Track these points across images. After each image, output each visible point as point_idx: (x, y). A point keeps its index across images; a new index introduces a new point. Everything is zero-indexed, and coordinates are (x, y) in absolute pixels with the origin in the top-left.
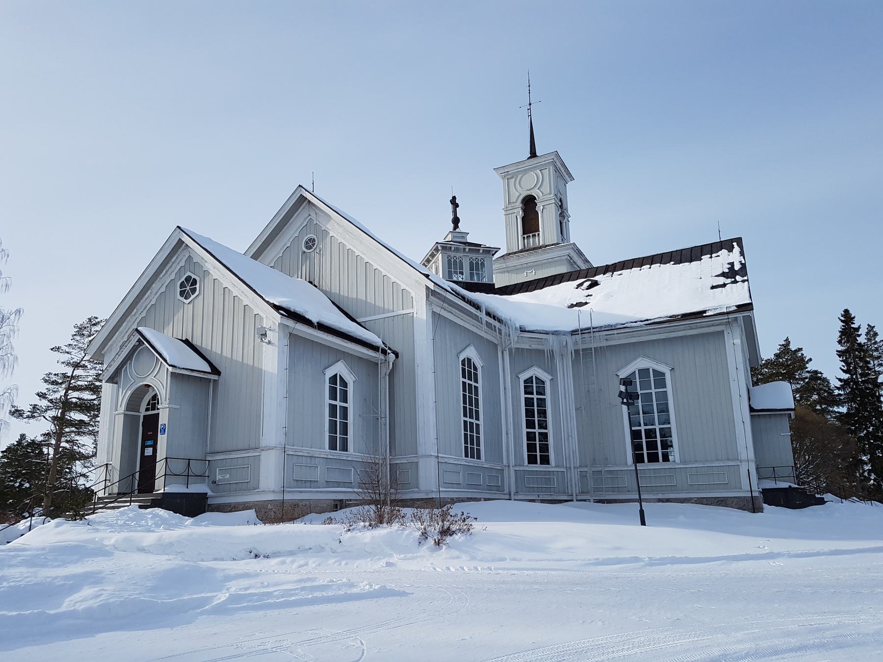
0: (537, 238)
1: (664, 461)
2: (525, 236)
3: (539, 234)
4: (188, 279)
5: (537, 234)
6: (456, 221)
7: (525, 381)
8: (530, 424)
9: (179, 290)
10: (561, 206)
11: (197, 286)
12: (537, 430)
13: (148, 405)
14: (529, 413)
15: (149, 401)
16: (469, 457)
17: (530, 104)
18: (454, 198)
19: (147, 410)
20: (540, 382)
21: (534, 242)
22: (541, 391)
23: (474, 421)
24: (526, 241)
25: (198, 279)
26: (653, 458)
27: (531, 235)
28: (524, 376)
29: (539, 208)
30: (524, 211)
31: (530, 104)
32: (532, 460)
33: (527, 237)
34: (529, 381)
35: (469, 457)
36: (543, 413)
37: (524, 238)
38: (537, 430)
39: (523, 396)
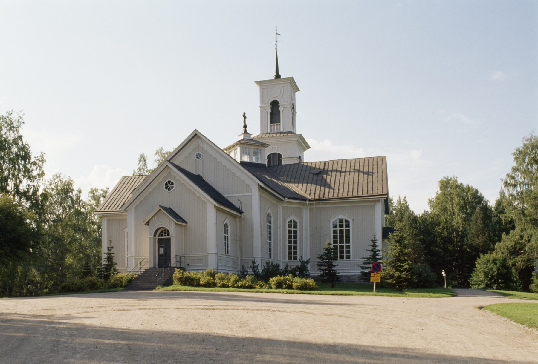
0: (279, 126)
1: (340, 259)
2: (272, 124)
3: (280, 124)
4: (169, 182)
5: (279, 124)
6: (245, 126)
7: (289, 222)
8: (290, 242)
9: (165, 186)
10: (293, 108)
11: (174, 185)
12: (293, 245)
13: (160, 234)
14: (290, 237)
15: (160, 233)
16: (292, 259)
17: (277, 42)
18: (244, 113)
19: (159, 236)
20: (295, 222)
21: (277, 128)
22: (295, 227)
23: (270, 241)
24: (272, 127)
25: (174, 183)
26: (342, 258)
27: (275, 124)
28: (288, 220)
29: (281, 109)
30: (272, 109)
31: (277, 42)
32: (290, 258)
33: (273, 125)
34: (290, 222)
35: (292, 259)
36: (295, 237)
37: (271, 125)
38: (293, 245)
39: (287, 229)
